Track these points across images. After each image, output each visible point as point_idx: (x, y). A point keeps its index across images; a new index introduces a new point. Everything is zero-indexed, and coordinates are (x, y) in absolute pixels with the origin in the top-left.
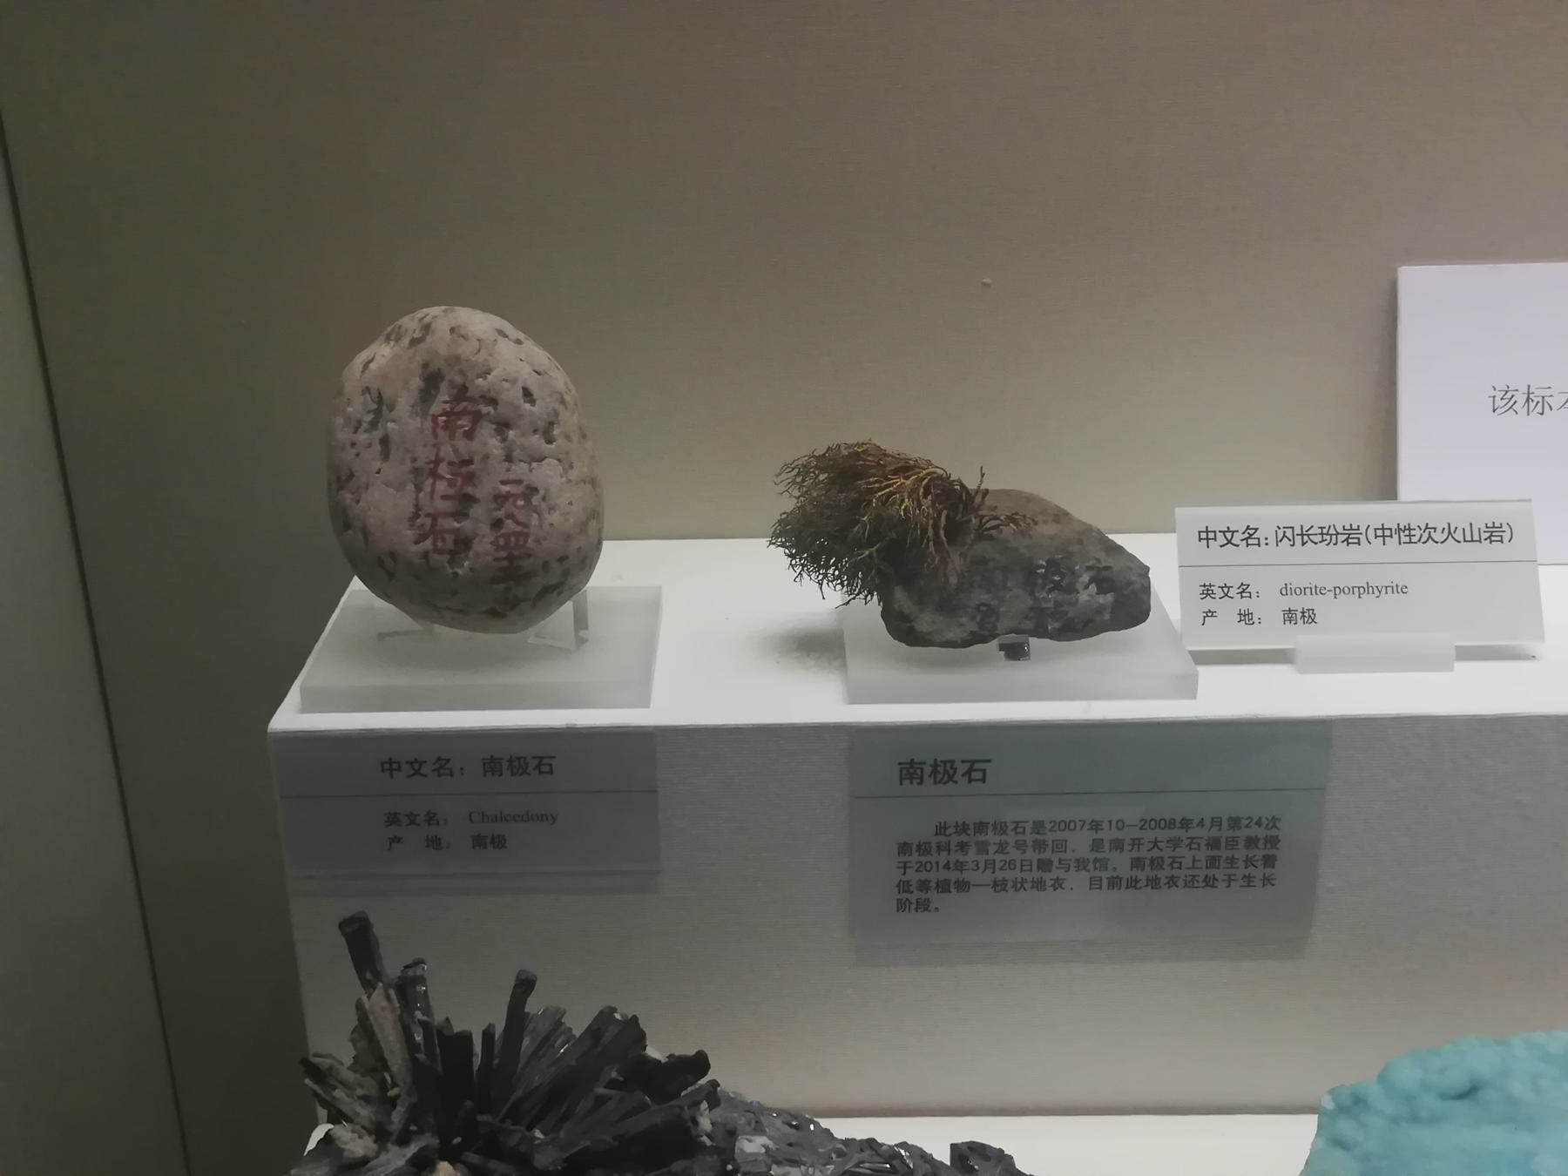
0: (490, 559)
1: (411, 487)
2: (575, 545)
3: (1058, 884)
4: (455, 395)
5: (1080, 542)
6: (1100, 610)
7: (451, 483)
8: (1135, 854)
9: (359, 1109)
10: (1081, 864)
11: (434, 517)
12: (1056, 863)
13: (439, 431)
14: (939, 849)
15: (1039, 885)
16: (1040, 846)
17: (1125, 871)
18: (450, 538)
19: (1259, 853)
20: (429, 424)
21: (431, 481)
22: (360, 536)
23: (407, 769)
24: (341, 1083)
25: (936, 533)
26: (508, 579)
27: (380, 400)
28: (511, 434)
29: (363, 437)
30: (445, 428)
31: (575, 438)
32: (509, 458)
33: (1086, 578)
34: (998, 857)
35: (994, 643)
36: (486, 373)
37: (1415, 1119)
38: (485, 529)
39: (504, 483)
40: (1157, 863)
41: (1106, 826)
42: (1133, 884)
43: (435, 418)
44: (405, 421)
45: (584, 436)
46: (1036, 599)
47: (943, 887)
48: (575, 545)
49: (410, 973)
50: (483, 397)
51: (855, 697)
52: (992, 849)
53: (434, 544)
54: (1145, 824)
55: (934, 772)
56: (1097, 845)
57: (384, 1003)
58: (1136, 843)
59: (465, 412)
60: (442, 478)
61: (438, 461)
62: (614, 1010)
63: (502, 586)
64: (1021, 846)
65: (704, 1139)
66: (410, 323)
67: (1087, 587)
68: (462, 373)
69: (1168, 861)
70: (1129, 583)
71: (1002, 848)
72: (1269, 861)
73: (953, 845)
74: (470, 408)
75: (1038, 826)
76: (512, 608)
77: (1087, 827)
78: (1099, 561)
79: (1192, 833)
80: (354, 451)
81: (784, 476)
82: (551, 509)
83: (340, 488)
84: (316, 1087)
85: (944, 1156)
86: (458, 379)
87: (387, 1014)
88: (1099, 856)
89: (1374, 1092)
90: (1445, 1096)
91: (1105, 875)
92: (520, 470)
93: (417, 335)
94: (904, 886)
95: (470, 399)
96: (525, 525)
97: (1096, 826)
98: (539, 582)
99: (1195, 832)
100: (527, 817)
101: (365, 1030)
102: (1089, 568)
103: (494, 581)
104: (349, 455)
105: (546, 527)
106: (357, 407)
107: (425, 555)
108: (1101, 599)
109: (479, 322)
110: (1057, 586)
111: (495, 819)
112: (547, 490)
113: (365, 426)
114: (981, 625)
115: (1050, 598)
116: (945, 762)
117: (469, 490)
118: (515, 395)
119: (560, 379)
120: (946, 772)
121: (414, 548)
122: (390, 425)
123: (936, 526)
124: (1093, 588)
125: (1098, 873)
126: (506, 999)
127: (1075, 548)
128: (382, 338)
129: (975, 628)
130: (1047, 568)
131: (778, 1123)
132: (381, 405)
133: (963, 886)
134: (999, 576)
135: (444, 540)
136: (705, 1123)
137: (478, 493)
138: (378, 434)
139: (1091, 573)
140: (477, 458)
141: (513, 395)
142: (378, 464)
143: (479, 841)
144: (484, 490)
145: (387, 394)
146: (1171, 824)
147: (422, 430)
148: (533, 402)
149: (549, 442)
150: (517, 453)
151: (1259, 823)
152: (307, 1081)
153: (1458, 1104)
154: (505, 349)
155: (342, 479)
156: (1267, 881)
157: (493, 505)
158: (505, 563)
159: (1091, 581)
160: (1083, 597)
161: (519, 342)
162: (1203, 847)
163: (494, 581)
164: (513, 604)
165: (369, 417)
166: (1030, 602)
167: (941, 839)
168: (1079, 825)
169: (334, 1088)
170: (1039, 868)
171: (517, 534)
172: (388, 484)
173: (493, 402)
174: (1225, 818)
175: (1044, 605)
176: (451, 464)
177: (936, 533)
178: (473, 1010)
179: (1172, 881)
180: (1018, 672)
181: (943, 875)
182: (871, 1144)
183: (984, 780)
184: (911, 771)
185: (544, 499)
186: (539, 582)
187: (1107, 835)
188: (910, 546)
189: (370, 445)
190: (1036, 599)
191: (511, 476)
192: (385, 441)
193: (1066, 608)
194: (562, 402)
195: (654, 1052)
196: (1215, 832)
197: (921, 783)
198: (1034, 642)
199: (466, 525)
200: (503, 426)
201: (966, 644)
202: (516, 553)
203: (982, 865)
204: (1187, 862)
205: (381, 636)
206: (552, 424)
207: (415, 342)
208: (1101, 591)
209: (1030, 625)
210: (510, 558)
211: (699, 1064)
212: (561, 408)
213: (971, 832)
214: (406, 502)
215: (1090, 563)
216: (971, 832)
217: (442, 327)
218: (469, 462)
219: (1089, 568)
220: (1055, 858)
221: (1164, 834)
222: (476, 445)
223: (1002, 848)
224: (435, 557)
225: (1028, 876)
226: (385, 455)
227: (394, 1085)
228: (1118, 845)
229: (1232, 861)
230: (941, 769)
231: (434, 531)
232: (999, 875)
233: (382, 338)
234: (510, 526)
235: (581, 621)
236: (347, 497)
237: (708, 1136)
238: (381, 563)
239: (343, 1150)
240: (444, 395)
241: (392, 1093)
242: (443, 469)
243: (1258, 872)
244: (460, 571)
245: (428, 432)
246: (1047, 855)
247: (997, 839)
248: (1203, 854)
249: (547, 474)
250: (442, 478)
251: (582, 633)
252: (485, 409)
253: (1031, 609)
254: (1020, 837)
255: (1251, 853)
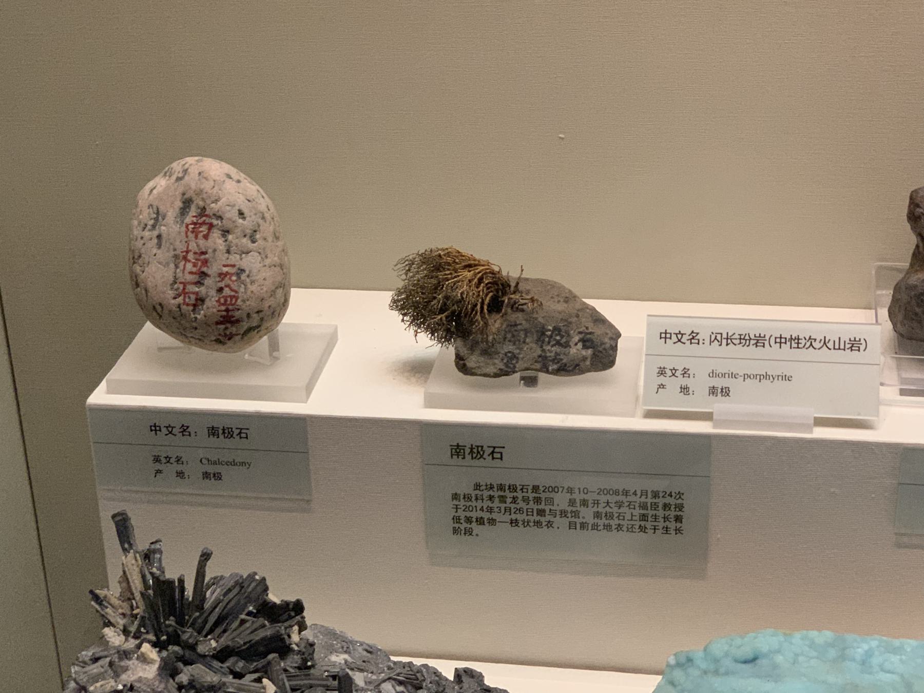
0: (215, 310)
1: (172, 266)
2: (266, 304)
3: (550, 524)
4: (201, 215)
5: (577, 316)
6: (584, 359)
7: (195, 265)
8: (595, 509)
9: (119, 620)
10: (563, 513)
11: (184, 284)
12: (548, 512)
13: (189, 233)
14: (477, 499)
15: (538, 524)
16: (538, 500)
17: (590, 520)
18: (193, 297)
19: (672, 513)
20: (184, 229)
21: (183, 263)
22: (143, 292)
23: (164, 430)
24: (111, 605)
25: (482, 308)
26: (229, 322)
27: (158, 213)
28: (230, 237)
29: (147, 234)
30: (192, 232)
31: (270, 239)
32: (228, 252)
33: (576, 338)
34: (513, 506)
35: (517, 375)
36: (216, 201)
37: (716, 673)
38: (213, 293)
39: (225, 266)
40: (609, 516)
41: (577, 491)
42: (595, 527)
43: (187, 226)
44: (171, 227)
45: (277, 238)
46: (543, 351)
47: (480, 521)
48: (266, 304)
49: (153, 546)
50: (214, 215)
51: (431, 402)
52: (509, 500)
53: (184, 300)
54: (601, 491)
55: (471, 452)
56: (572, 502)
57: (134, 562)
58: (596, 503)
59: (204, 223)
60: (189, 261)
61: (187, 252)
62: (256, 574)
63: (223, 327)
64: (526, 500)
65: (294, 646)
66: (177, 166)
67: (576, 344)
68: (203, 199)
69: (616, 515)
70: (603, 344)
71: (515, 500)
72: (678, 519)
73: (493, 496)
74: (207, 221)
75: (535, 489)
76: (229, 339)
77: (565, 490)
78: (587, 328)
79: (630, 499)
80: (142, 242)
81: (399, 266)
82: (252, 282)
83: (134, 263)
84: (97, 607)
85: (451, 677)
86: (201, 203)
87: (135, 567)
88: (574, 509)
89: (699, 655)
90: (736, 661)
91: (578, 521)
92: (234, 258)
93: (180, 175)
94: (457, 519)
95: (206, 216)
96: (236, 292)
97: (570, 490)
98: (245, 325)
99: (632, 498)
100: (234, 463)
101: (125, 578)
102: (580, 333)
103: (217, 323)
104: (139, 244)
105: (249, 293)
106: (146, 215)
107: (179, 306)
108: (584, 353)
109: (215, 168)
110: (558, 343)
111: (215, 463)
112: (250, 272)
113: (149, 227)
114: (506, 365)
115: (552, 350)
116: (478, 447)
117: (205, 269)
118: (234, 214)
119: (264, 203)
120: (478, 452)
121: (173, 301)
122: (163, 228)
123: (483, 303)
124: (580, 345)
125: (573, 519)
126: (196, 563)
127: (574, 320)
128: (162, 174)
129: (503, 367)
130: (553, 332)
131: (360, 649)
132: (158, 216)
133: (492, 522)
134: (522, 335)
135: (189, 298)
136: (295, 638)
137: (209, 272)
138: (156, 233)
139: (581, 336)
140: (210, 251)
141: (232, 214)
142: (155, 251)
143: (206, 475)
144: (213, 270)
145: (162, 208)
146: (616, 492)
147: (180, 232)
148: (244, 218)
149: (253, 242)
150: (233, 249)
151: (635, 493)
152: (93, 603)
153: (743, 666)
154: (229, 186)
155: (136, 258)
156: (678, 531)
157: (218, 279)
158: (224, 313)
159: (579, 341)
160: (573, 351)
161: (239, 181)
162: (637, 508)
163: (217, 323)
164: (230, 337)
165: (152, 222)
166: (539, 352)
167: (477, 492)
168: (560, 489)
169: (107, 607)
170: (538, 514)
171: (231, 297)
172: (160, 263)
173: (220, 218)
174: (621, 490)
175: (548, 354)
176: (195, 253)
177: (482, 308)
178: (178, 567)
179: (619, 527)
180: (530, 394)
181: (480, 514)
182: (401, 662)
183: (501, 459)
184: (457, 451)
185: (248, 276)
186: (245, 325)
187: (578, 497)
188: (470, 312)
189: (151, 239)
190: (543, 351)
191: (229, 262)
192: (159, 237)
193: (562, 357)
194: (263, 218)
195: (274, 597)
196: (643, 499)
197: (464, 458)
198: (542, 376)
199: (202, 290)
200: (226, 232)
201: (496, 376)
202: (230, 307)
203: (503, 511)
204: (628, 517)
205: (160, 349)
206: (255, 231)
207: (179, 179)
208: (585, 347)
209: (538, 366)
210: (227, 310)
211: (298, 607)
212: (261, 221)
213: (495, 489)
214: (169, 274)
215: (581, 330)
216: (495, 489)
217: (194, 171)
218: (203, 253)
219: (580, 333)
220: (547, 508)
221: (613, 499)
222: (210, 242)
223: (515, 500)
224: (184, 307)
225: (532, 518)
226: (159, 246)
227: (138, 607)
228: (584, 503)
229: (655, 518)
230: (475, 450)
231: (184, 293)
232: (514, 517)
233: (162, 174)
234: (227, 291)
235: (274, 346)
236: (138, 269)
237: (297, 645)
238: (154, 308)
239: (108, 642)
240: (193, 211)
241: (135, 612)
242: (191, 256)
243: (672, 525)
244: (199, 317)
245: (183, 234)
246: (541, 507)
247: (512, 495)
248: (637, 512)
249: (251, 262)
250: (189, 261)
251: (275, 354)
252: (215, 222)
253: (540, 356)
254: (524, 494)
255: (667, 513)
